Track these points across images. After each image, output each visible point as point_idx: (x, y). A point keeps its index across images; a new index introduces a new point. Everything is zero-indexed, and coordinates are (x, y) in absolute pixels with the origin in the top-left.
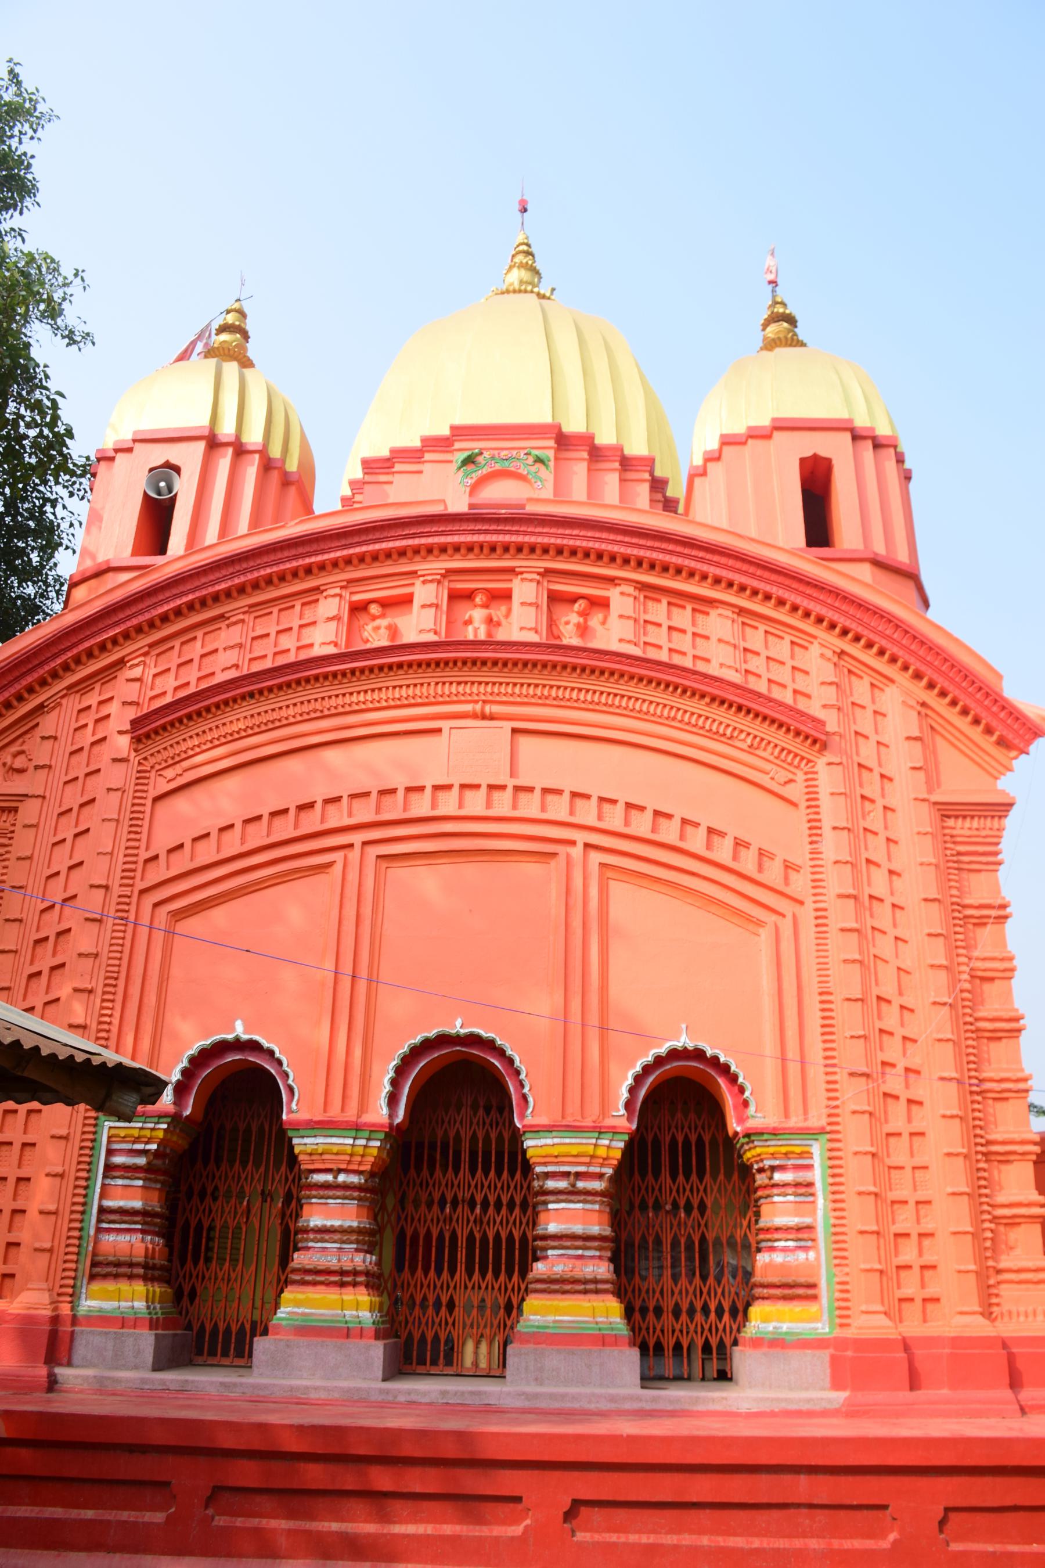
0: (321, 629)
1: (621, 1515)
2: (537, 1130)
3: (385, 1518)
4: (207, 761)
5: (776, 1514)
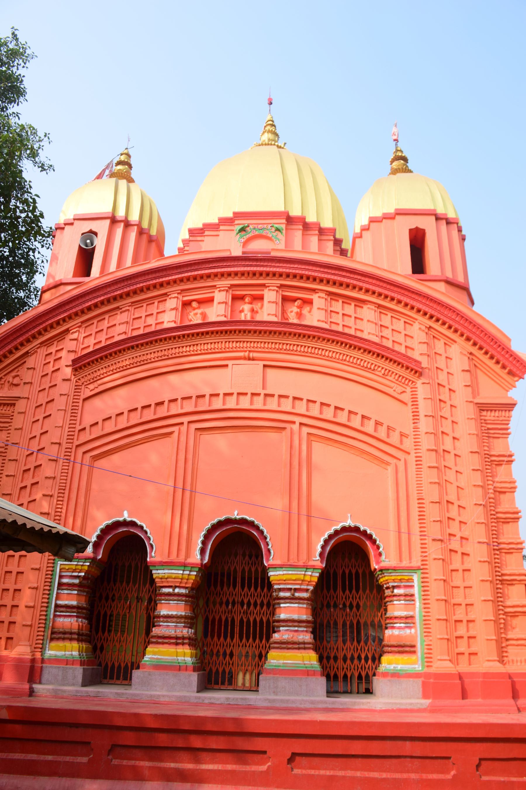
1: (316, 761)
2: (275, 567)
3: (198, 761)
5: (394, 761)
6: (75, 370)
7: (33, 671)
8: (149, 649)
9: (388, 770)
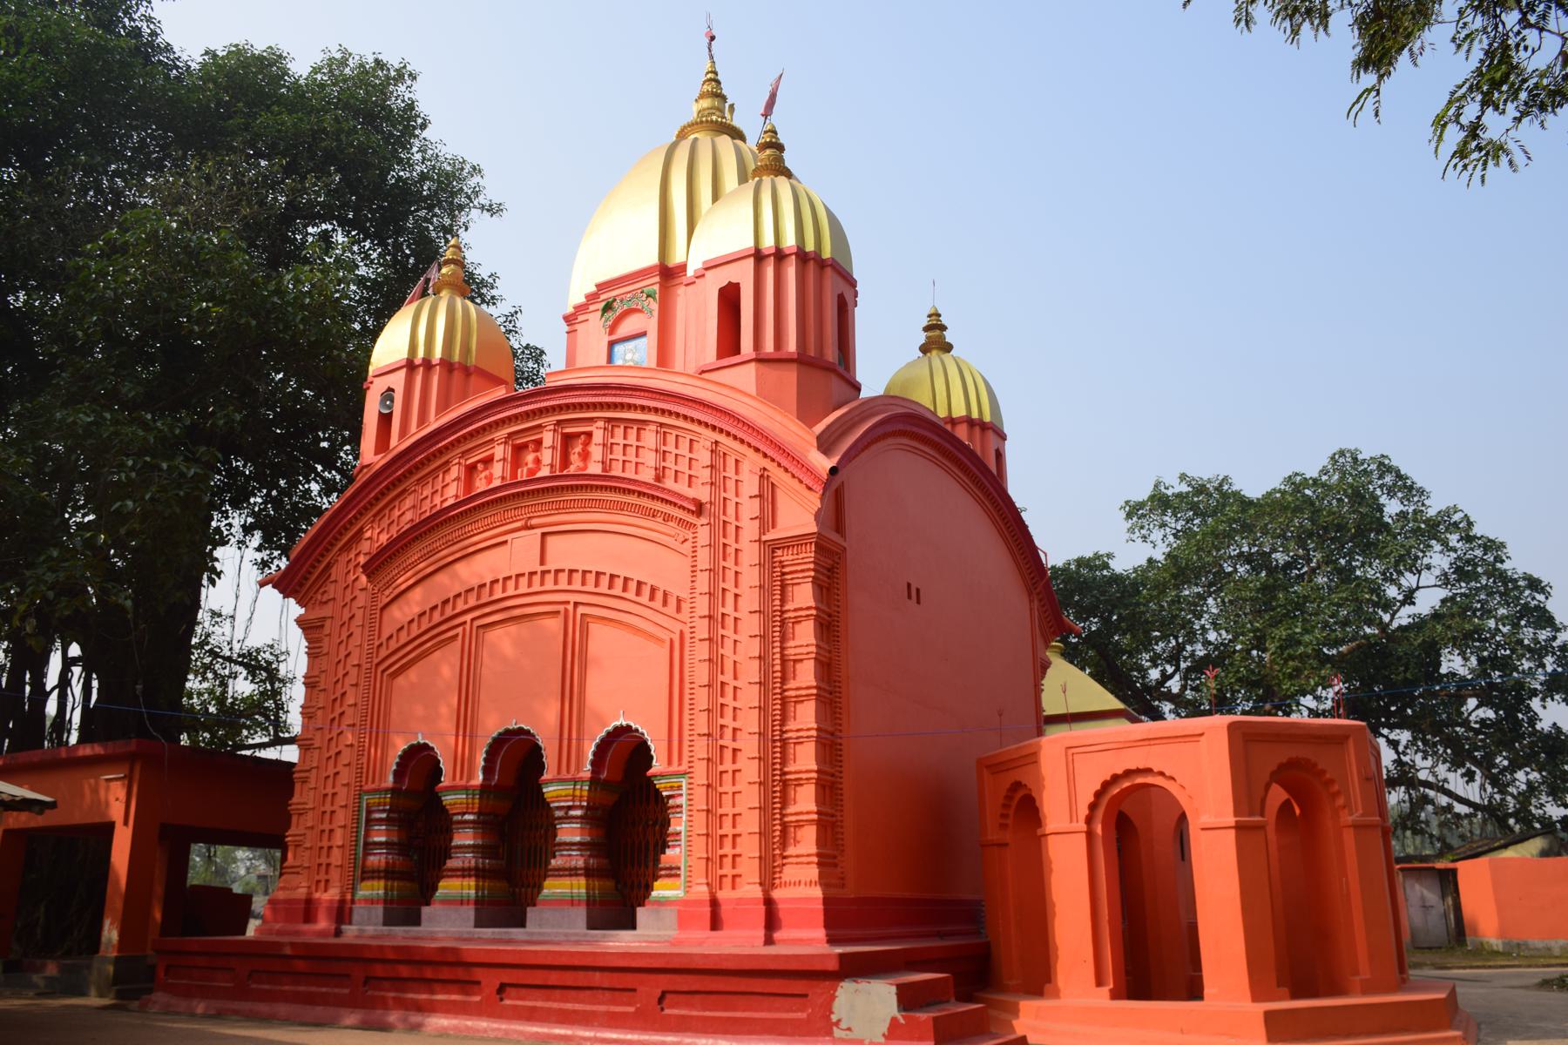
0: (450, 490)
1: (523, 991)
3: (432, 992)
4: (403, 581)
5: (588, 993)
6: (368, 576)
7: (342, 913)
8: (441, 884)
9: (769, 1010)
